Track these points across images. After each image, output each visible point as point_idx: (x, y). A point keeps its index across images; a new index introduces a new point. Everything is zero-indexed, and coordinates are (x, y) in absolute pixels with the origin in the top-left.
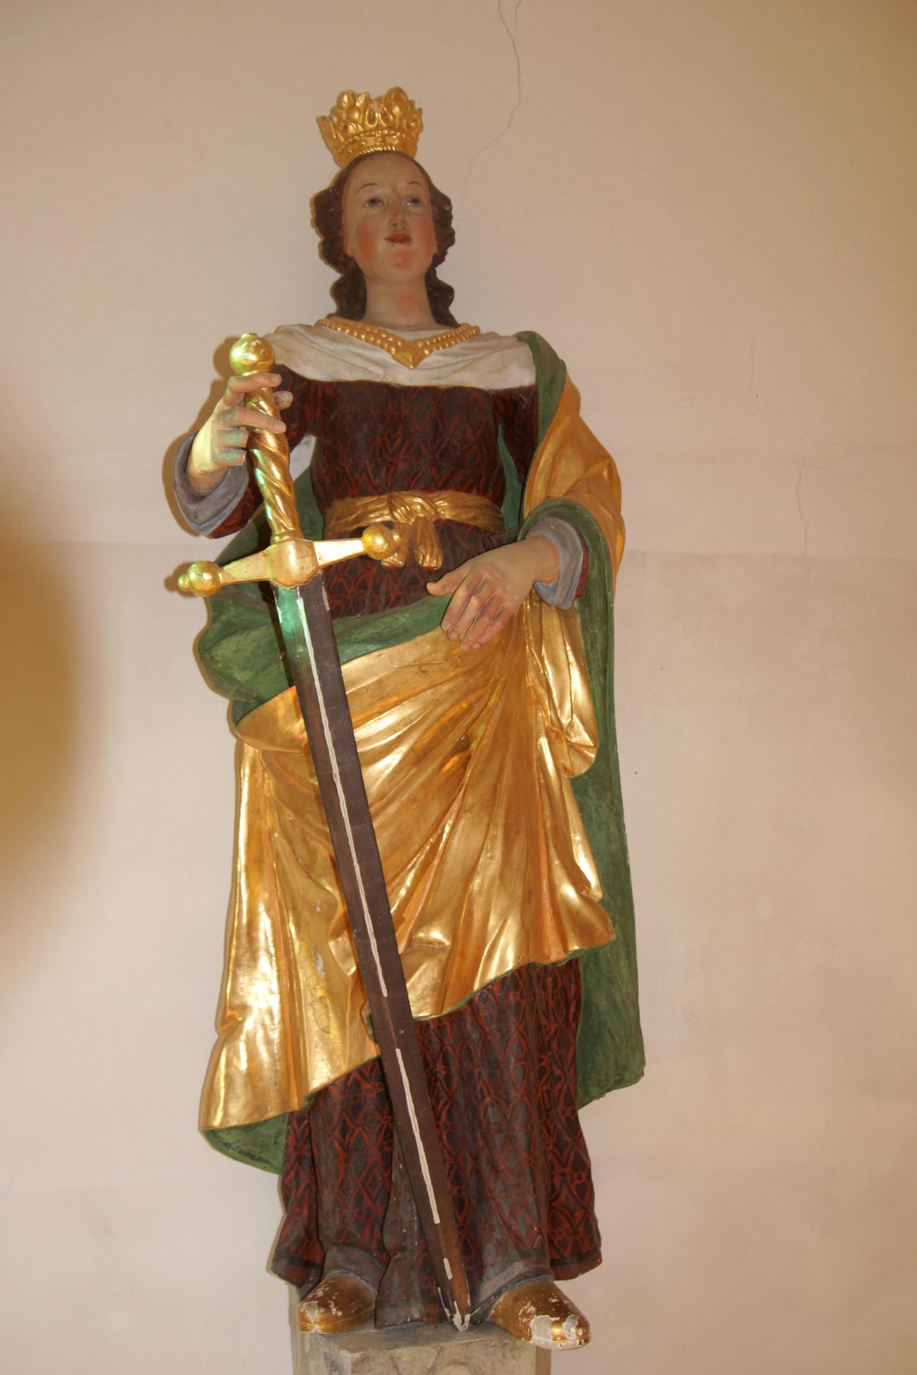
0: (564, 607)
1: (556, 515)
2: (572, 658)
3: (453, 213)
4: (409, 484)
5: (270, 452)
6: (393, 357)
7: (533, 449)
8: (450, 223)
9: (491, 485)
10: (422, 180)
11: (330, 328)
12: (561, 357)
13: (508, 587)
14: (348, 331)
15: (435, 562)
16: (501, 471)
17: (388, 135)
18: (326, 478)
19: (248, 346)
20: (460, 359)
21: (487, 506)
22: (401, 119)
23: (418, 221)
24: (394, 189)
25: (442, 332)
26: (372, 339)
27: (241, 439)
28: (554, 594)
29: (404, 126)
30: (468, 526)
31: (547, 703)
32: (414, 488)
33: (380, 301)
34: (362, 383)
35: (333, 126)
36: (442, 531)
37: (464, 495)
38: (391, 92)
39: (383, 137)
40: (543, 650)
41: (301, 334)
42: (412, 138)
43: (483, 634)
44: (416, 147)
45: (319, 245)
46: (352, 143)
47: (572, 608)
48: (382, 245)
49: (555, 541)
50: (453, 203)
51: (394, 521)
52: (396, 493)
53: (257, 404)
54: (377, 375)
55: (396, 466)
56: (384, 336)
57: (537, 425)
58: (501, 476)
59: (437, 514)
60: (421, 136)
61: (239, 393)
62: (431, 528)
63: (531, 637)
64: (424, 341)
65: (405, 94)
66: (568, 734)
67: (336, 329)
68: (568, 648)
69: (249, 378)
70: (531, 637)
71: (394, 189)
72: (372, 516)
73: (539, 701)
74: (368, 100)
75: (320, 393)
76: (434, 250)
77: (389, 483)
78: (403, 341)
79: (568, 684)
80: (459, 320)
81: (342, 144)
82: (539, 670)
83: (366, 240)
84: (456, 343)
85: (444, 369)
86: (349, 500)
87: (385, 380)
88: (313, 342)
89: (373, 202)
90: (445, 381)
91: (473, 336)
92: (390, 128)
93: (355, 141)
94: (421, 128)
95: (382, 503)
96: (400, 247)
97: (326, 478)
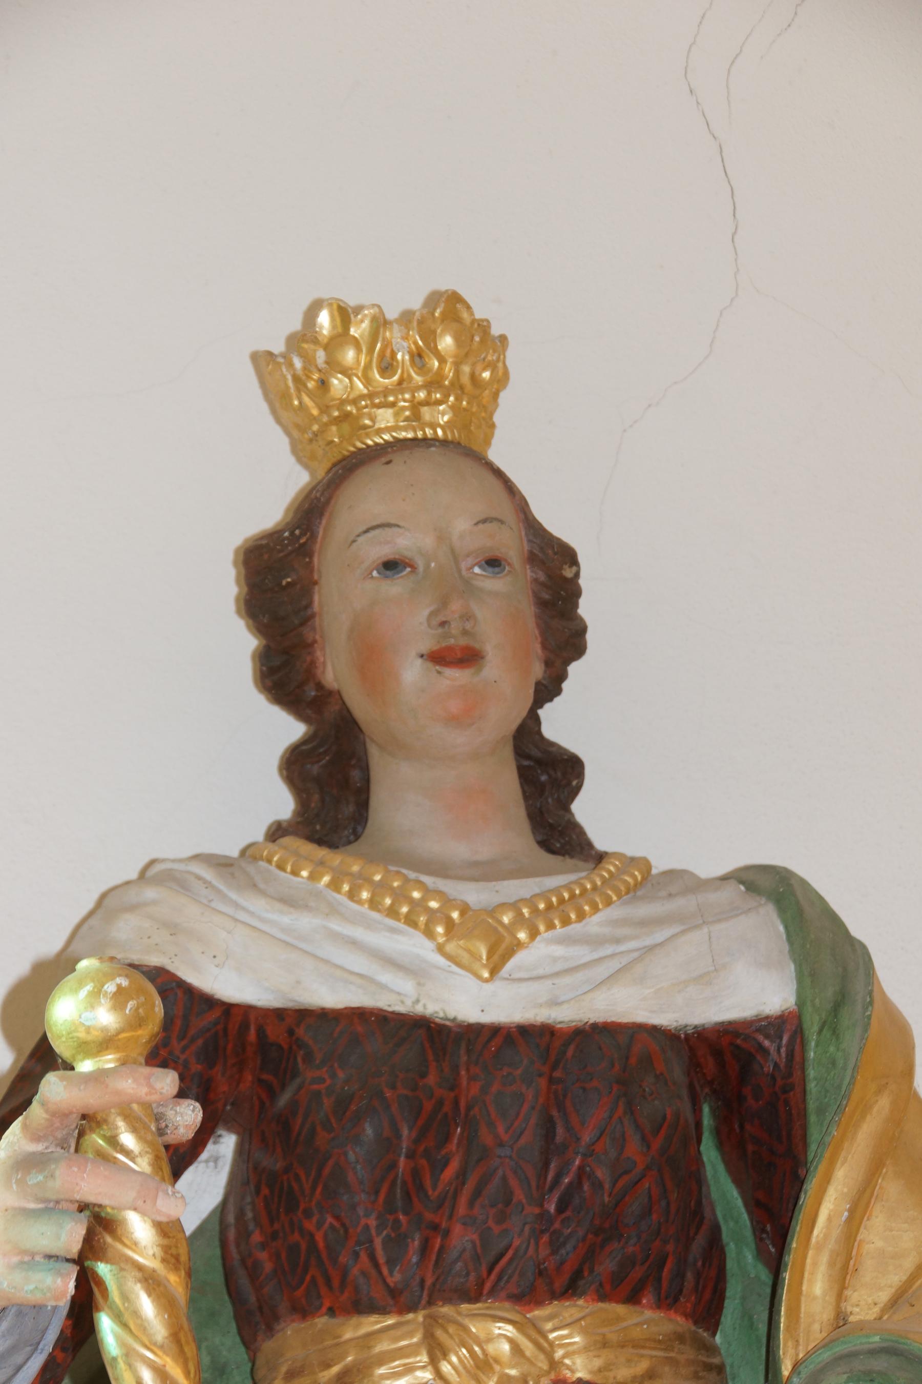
3: (583, 582)
4: (481, 1284)
5: (140, 1268)
6: (440, 949)
7: (797, 1182)
8: (576, 606)
9: (690, 1276)
10: (506, 510)
11: (281, 867)
12: (855, 931)
14: (326, 879)
16: (716, 1230)
17: (426, 403)
18: (263, 1256)
19: (97, 993)
20: (609, 950)
21: (680, 1338)
22: (457, 365)
23: (499, 613)
24: (442, 537)
25: (560, 879)
26: (388, 901)
27: (70, 1235)
29: (465, 380)
32: (492, 1293)
33: (404, 800)
34: (359, 1015)
35: (292, 377)
37: (621, 1309)
38: (434, 298)
39: (416, 406)
41: (208, 884)
42: (485, 408)
44: (493, 426)
45: (254, 657)
46: (337, 421)
48: (412, 673)
50: (581, 559)
52: (446, 1310)
53: (113, 1141)
54: (399, 995)
55: (447, 1233)
56: (416, 895)
57: (803, 1114)
58: (715, 1249)
59: (554, 1365)
60: (503, 396)
61: (65, 1115)
64: (515, 906)
65: (468, 307)
67: (295, 873)
69: (98, 1077)
71: (442, 537)
72: (382, 1371)
74: (380, 323)
75: (252, 1035)
76: (538, 671)
77: (429, 1282)
78: (465, 909)
80: (600, 837)
81: (315, 419)
83: (372, 656)
84: (595, 909)
85: (567, 980)
86: (321, 1321)
87: (419, 1009)
88: (237, 905)
89: (391, 566)
90: (567, 1013)
91: (637, 885)
92: (429, 386)
93: (347, 416)
94: (502, 380)
95: (410, 1335)
96: (455, 676)
97: (263, 1256)
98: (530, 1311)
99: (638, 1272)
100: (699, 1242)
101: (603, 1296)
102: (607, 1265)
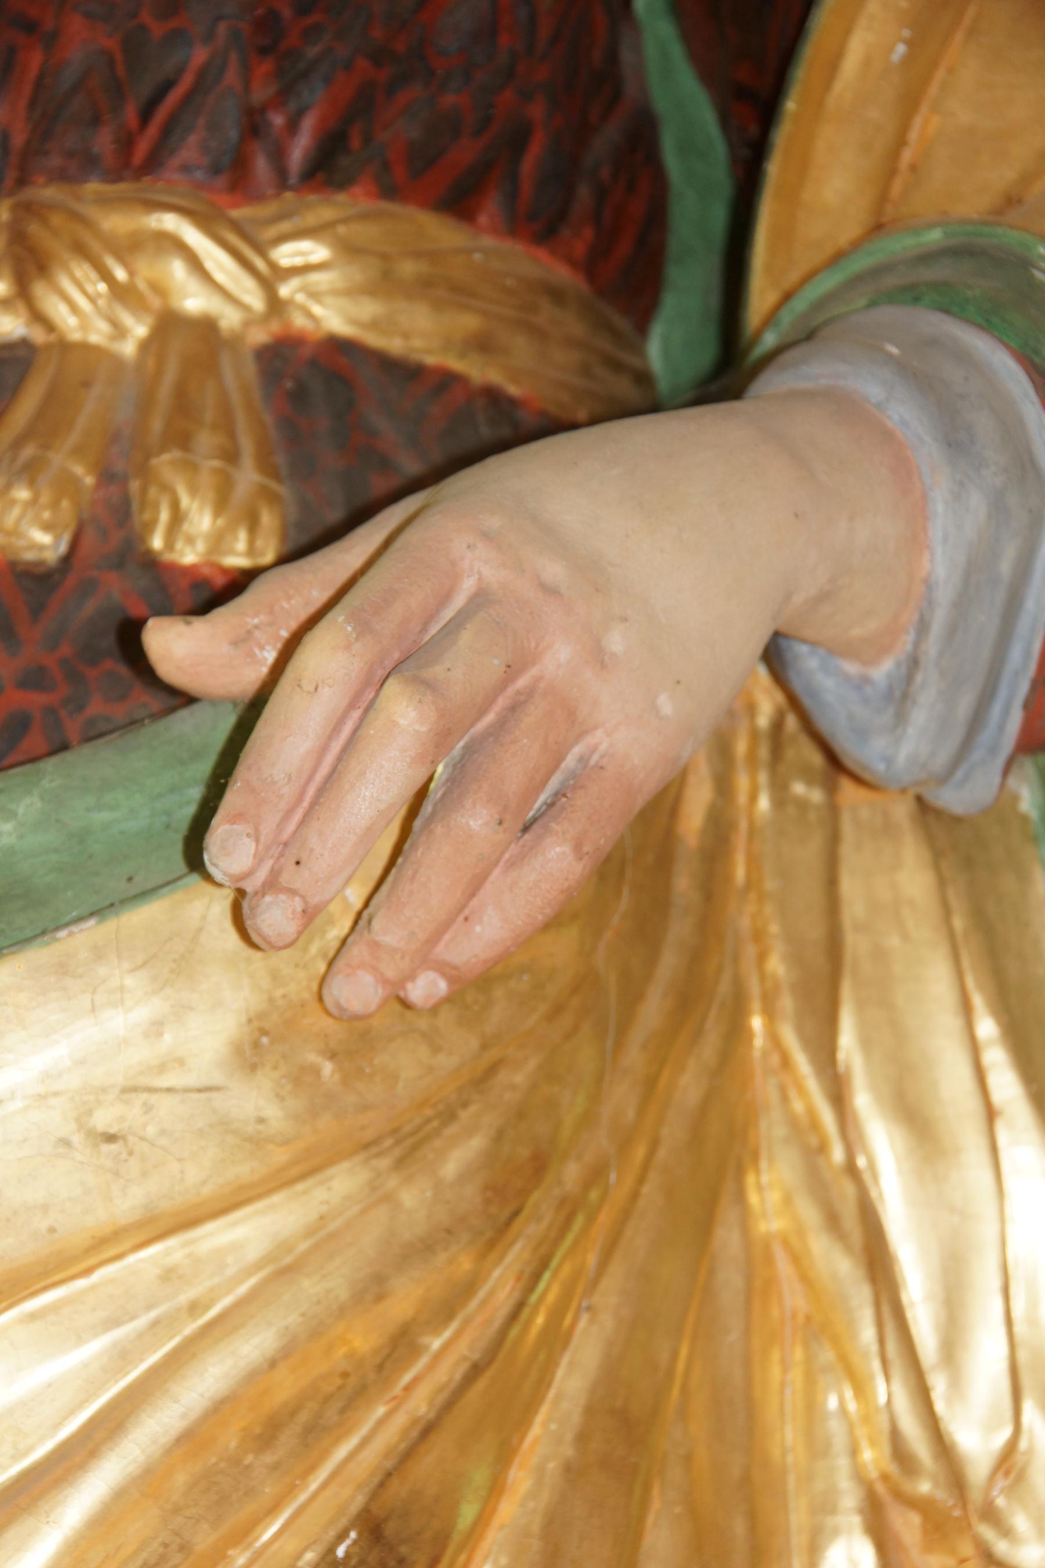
0: (953, 799)
1: (912, 294)
2: (1006, 1085)
9: (584, 193)
13: (616, 642)
15: (241, 543)
28: (901, 718)
30: (446, 381)
31: (868, 1334)
36: (299, 396)
40: (847, 1039)
43: (460, 913)
47: (1002, 808)
49: (904, 414)
51: (39, 336)
52: (49, 193)
59: (276, 305)
62: (238, 378)
63: (776, 965)
66: (990, 1514)
68: (987, 1027)
70: (776, 965)
73: (822, 1327)
79: (989, 1232)
82: (823, 1148)
98: (236, 205)
99: (465, 152)
100: (607, 138)
101: (390, 191)
102: (401, 127)
